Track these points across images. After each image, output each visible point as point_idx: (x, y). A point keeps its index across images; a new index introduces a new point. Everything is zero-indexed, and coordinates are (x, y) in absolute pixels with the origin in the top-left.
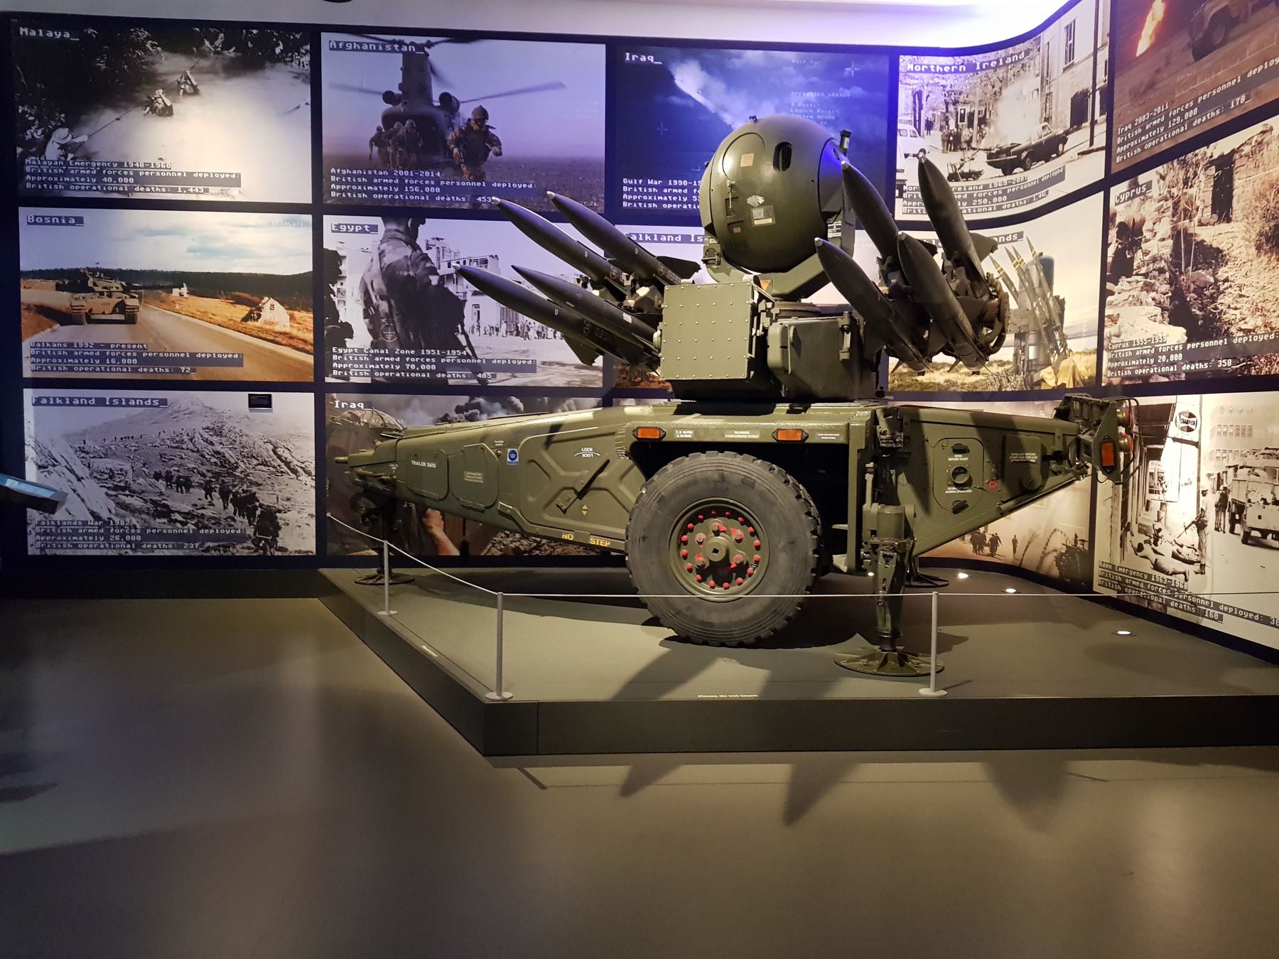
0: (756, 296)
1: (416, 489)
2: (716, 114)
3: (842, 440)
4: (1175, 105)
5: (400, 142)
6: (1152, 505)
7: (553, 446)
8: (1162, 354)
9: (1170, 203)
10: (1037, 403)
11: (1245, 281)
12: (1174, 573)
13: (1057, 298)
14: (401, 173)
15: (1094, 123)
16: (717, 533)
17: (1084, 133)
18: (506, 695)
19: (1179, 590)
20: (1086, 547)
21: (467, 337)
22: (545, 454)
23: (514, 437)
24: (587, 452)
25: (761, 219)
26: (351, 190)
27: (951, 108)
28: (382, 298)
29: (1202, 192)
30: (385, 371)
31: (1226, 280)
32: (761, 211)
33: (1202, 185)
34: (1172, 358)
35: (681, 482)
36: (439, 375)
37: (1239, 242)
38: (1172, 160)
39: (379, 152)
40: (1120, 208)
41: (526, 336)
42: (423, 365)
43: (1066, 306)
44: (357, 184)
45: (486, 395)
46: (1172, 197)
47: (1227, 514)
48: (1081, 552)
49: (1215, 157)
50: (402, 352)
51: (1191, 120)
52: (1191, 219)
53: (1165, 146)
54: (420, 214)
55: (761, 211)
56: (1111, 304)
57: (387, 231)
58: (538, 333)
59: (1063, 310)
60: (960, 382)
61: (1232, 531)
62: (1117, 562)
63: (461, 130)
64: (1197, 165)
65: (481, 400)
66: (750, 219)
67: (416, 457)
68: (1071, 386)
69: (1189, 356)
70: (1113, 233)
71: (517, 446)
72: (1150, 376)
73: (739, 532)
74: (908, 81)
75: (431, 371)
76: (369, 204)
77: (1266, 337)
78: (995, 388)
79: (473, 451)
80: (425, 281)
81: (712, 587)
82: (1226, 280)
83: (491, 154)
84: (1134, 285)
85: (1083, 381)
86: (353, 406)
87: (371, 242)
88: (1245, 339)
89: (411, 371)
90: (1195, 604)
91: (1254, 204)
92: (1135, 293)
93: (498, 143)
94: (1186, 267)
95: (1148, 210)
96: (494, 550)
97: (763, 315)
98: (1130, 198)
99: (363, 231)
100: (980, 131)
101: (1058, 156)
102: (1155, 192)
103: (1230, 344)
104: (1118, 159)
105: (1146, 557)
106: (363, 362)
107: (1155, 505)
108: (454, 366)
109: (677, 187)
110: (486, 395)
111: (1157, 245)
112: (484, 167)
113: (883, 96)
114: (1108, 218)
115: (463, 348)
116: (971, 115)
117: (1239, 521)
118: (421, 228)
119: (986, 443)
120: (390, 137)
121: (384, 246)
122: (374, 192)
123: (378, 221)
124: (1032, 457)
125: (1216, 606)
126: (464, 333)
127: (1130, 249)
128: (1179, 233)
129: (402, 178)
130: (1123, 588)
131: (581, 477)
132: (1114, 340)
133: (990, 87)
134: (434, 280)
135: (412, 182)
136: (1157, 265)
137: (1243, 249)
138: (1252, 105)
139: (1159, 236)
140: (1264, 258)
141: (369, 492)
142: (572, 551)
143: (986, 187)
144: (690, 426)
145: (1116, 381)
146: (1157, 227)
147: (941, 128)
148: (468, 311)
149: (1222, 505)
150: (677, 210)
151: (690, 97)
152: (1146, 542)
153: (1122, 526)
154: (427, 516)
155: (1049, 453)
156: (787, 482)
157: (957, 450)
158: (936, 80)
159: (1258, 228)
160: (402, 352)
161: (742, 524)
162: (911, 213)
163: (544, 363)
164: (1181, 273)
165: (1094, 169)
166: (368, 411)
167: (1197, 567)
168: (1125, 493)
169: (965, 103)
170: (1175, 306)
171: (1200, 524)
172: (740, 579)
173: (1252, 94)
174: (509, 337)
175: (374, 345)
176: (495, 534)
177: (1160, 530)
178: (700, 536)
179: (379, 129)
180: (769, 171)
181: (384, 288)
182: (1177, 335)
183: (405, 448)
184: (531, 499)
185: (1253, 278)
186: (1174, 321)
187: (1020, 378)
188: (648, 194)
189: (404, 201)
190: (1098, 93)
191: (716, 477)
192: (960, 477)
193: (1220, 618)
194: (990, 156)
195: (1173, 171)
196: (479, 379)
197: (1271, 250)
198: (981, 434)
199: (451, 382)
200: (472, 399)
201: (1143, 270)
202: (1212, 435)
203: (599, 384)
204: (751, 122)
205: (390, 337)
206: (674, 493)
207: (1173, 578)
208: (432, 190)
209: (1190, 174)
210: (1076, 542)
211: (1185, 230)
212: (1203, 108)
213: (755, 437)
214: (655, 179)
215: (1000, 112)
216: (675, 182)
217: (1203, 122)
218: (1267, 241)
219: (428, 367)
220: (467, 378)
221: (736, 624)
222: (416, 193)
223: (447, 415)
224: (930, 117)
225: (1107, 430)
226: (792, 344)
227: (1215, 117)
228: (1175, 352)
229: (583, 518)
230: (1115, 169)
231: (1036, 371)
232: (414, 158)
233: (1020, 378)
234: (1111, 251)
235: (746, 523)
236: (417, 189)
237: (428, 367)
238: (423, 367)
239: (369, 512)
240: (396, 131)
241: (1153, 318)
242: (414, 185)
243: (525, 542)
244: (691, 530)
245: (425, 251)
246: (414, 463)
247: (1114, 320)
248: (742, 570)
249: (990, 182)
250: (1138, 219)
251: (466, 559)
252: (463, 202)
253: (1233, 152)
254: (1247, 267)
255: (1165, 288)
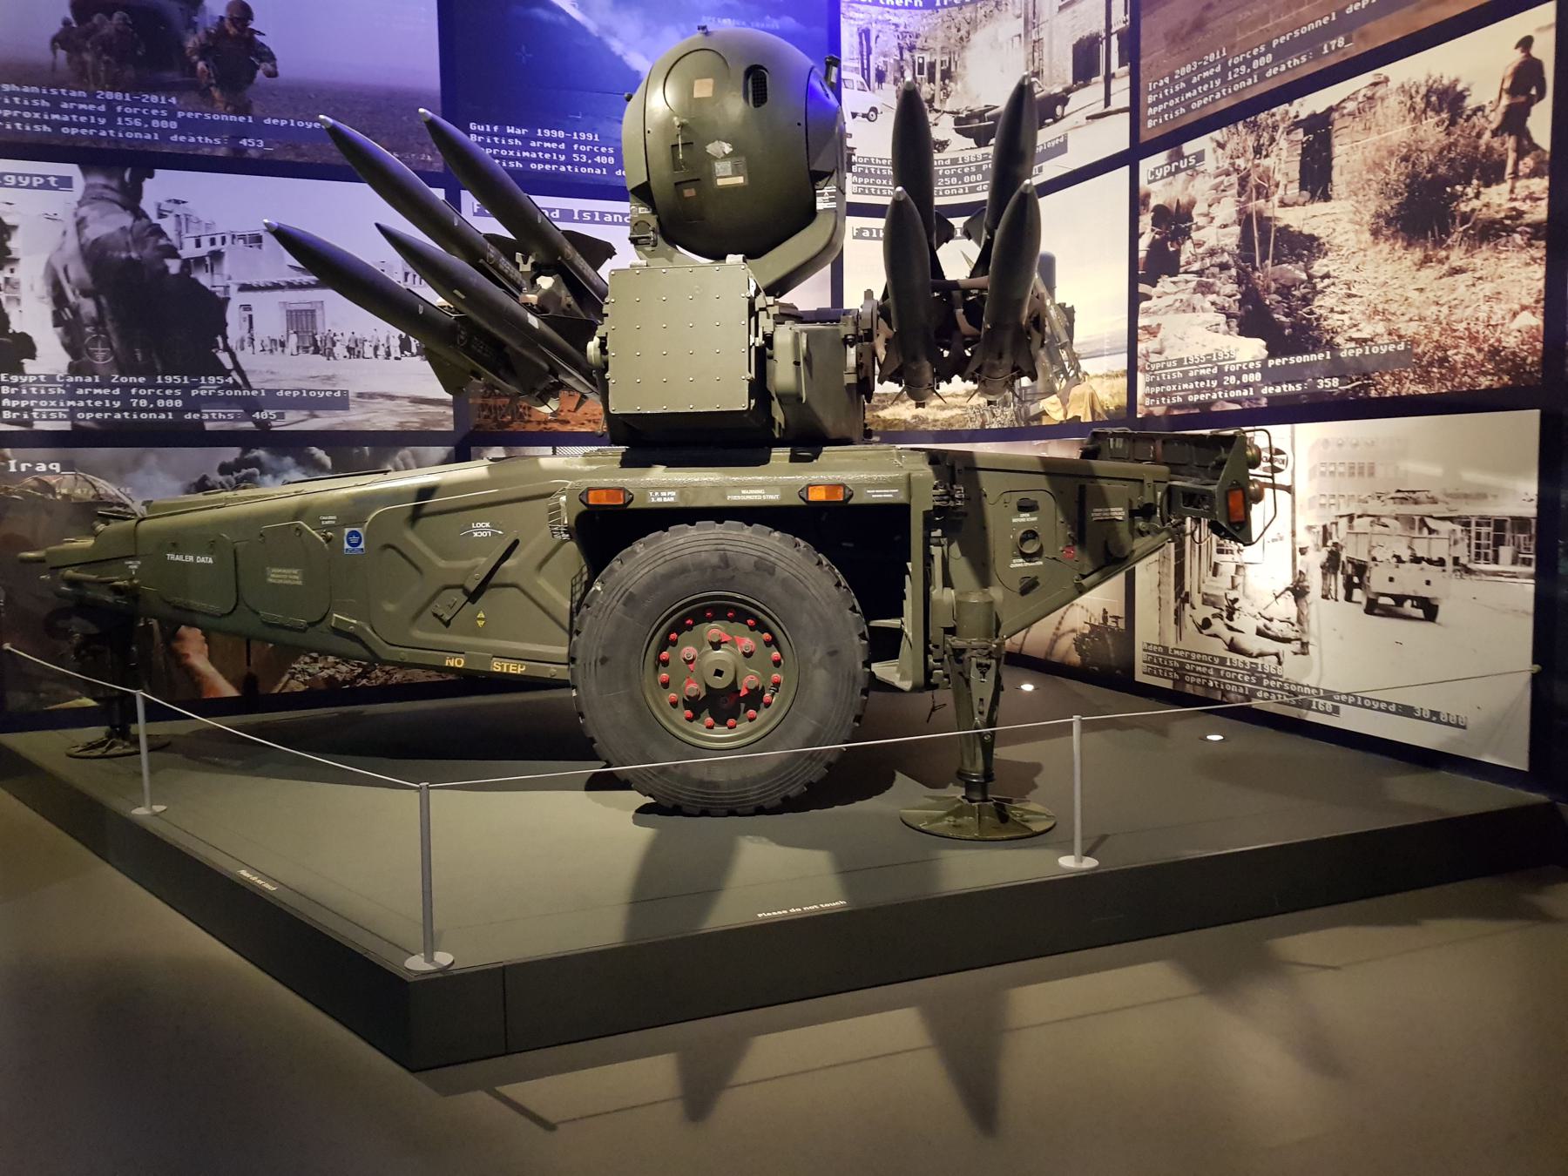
0: (753, 289)
1: (178, 600)
2: (599, 39)
3: (902, 499)
4: (1236, 50)
5: (106, 46)
6: (1221, 569)
7: (423, 521)
8: (1229, 373)
9: (1234, 178)
10: (1036, 443)
11: (1356, 276)
12: (1261, 655)
13: (1062, 306)
14: (109, 95)
15: (1109, 78)
16: (716, 646)
17: (1095, 90)
18: (443, 958)
19: (1269, 676)
20: (1122, 624)
21: (233, 356)
22: (410, 535)
23: (356, 509)
24: (481, 529)
25: (727, 177)
26: (20, 119)
27: (907, 55)
28: (85, 294)
29: (1284, 161)
30: (95, 410)
31: (1327, 276)
32: (728, 164)
33: (1284, 154)
34: (1245, 378)
35: (660, 570)
36: (188, 416)
37: (1344, 225)
38: (1235, 122)
39: (69, 60)
40: (1154, 187)
41: (330, 354)
42: (160, 399)
43: (1076, 316)
44: (31, 109)
45: (269, 444)
46: (1237, 171)
47: (1340, 577)
48: (1114, 633)
49: (1303, 116)
50: (124, 380)
51: (1262, 71)
52: (1267, 198)
53: (1223, 105)
54: (147, 161)
55: (728, 164)
56: (1147, 311)
57: (88, 187)
58: (349, 349)
59: (1071, 321)
60: (931, 418)
61: (1348, 598)
62: (1171, 643)
63: (208, 33)
64: (1275, 128)
65: (261, 453)
66: (711, 176)
67: (175, 548)
68: (1089, 419)
69: (1271, 376)
70: (1146, 221)
71: (361, 523)
72: (1211, 403)
73: (748, 642)
74: (852, 14)
75: (174, 410)
76: (56, 142)
77: (1391, 348)
78: (977, 425)
79: (281, 536)
80: (160, 267)
81: (710, 727)
82: (1327, 276)
83: (260, 73)
84: (1182, 286)
85: (1107, 412)
86: (42, 467)
87: (64, 203)
88: (1359, 352)
89: (140, 410)
90: (1295, 694)
91: (1366, 176)
92: (1184, 296)
93: (271, 57)
94: (1263, 260)
95: (1200, 189)
96: (293, 683)
97: (762, 315)
98: (1170, 174)
99: (46, 186)
100: (944, 87)
101: (1056, 121)
102: (1209, 164)
103: (1336, 359)
104: (1150, 123)
105: (1216, 636)
106: (56, 397)
107: (1228, 568)
108: (213, 401)
109: (551, 140)
110: (269, 444)
111: (1216, 229)
112: (249, 92)
113: (821, 32)
114: (1137, 201)
115: (227, 374)
116: (932, 65)
117: (1359, 586)
118: (147, 184)
119: (1058, 495)
120: (87, 36)
121: (84, 211)
122: (64, 124)
123: (71, 170)
124: (1119, 513)
125: (1329, 695)
126: (227, 349)
127: (1174, 239)
128: (1249, 217)
129: (111, 104)
130: (1182, 677)
131: (473, 568)
132: (1154, 358)
133: (954, 30)
134: (174, 266)
135: (128, 110)
136: (1217, 260)
137: (1351, 235)
138: (1355, 49)
139: (1217, 222)
140: (1385, 247)
141: (84, 607)
142: (420, 676)
143: (954, 161)
144: (663, 484)
145: (1159, 411)
146: (1214, 210)
147: (896, 81)
148: (233, 315)
149: (1332, 564)
150: (550, 173)
151: (561, 11)
152: (1214, 616)
153: (1177, 596)
154: (181, 638)
155: (1135, 507)
156: (820, 563)
157: (1026, 507)
158: (887, 17)
159: (1372, 207)
160: (124, 380)
161: (752, 628)
162: (863, 193)
163: (360, 395)
164: (1255, 269)
165: (1115, 136)
166: (69, 476)
167: (1296, 646)
168: (1180, 555)
169: (923, 49)
170: (1247, 312)
171: (1298, 591)
172: (751, 712)
173: (1355, 35)
174: (303, 355)
175: (73, 369)
176: (295, 660)
177: (1236, 600)
178: (689, 651)
179: (66, 23)
180: (735, 106)
181: (86, 276)
182: (1252, 349)
183: (153, 533)
184: (390, 607)
185: (1368, 272)
186: (1246, 331)
187: (1009, 411)
188: (508, 148)
189: (116, 140)
190: (1114, 39)
191: (715, 560)
192: (1028, 543)
193: (1336, 710)
194: (958, 121)
195: (1238, 137)
196: (255, 421)
197: (1394, 236)
198: (1052, 484)
199: (209, 426)
200: (246, 450)
201: (1196, 267)
202: (1312, 476)
203: (449, 426)
204: (699, 35)
205: (101, 355)
206: (650, 588)
207: (1259, 661)
208: (164, 124)
209: (1265, 139)
210: (1105, 619)
211: (1259, 213)
212: (1281, 54)
213: (773, 498)
214: (517, 126)
215: (968, 63)
216: (547, 133)
217: (1278, 74)
218: (1389, 223)
219: (170, 403)
220: (236, 419)
221: (754, 781)
222: (135, 129)
223: (205, 478)
224: (882, 67)
225: (1194, 469)
226: (805, 359)
227: (1302, 66)
228: (1249, 371)
229: (477, 632)
230: (1145, 136)
231: (1033, 402)
232: (130, 73)
233: (1009, 411)
234: (1144, 243)
235: (760, 626)
236: (137, 122)
237: (170, 403)
238: (160, 403)
239: (88, 639)
240: (95, 29)
241: (1214, 328)
242: (133, 116)
243: (344, 668)
244: (674, 643)
245: (155, 220)
246: (171, 556)
247: (1152, 332)
248: (755, 698)
249: (959, 155)
250: (1184, 200)
251: (252, 698)
252: (217, 146)
253: (1331, 110)
254: (1359, 257)
255: (1231, 288)
